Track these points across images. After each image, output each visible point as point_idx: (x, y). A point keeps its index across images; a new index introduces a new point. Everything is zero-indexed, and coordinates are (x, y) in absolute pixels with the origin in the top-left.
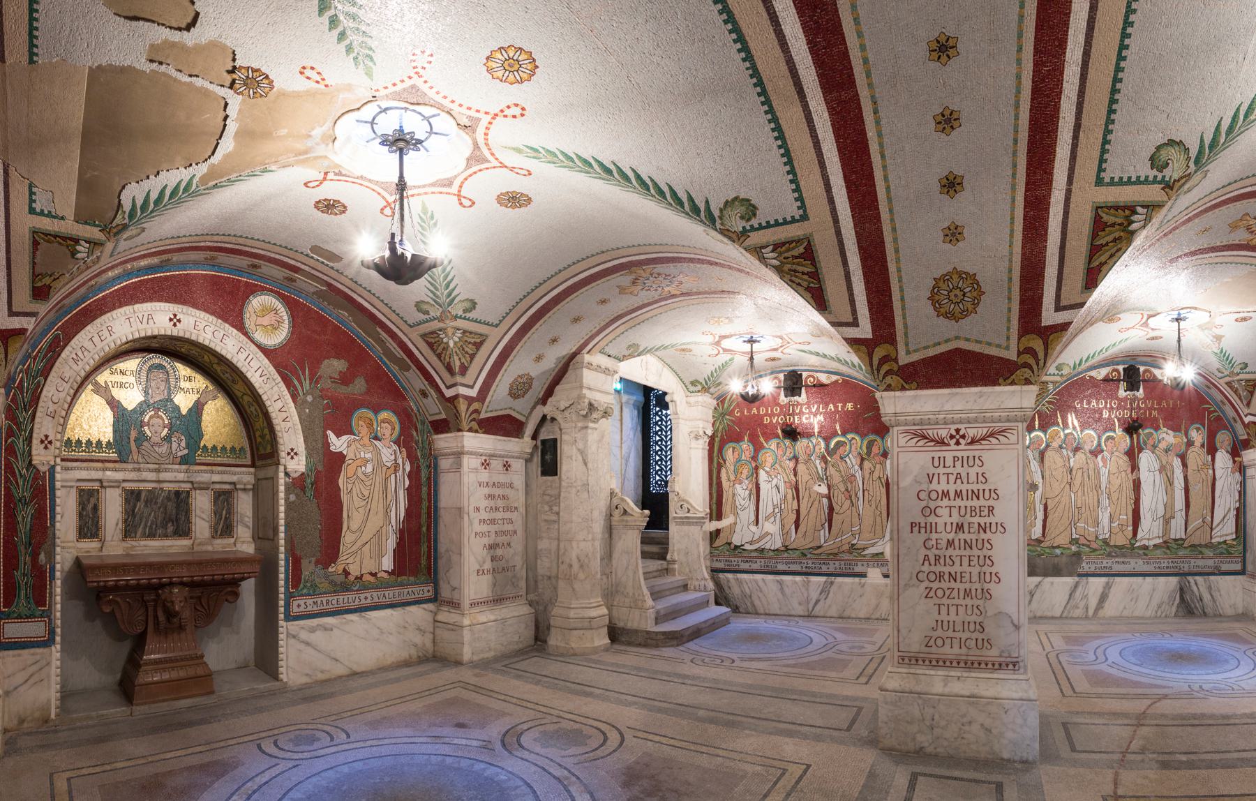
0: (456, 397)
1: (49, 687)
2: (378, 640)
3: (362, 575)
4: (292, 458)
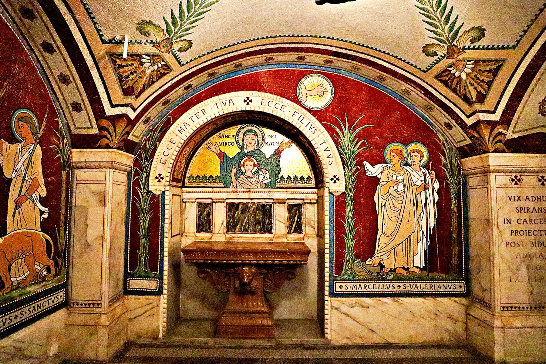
0: (479, 122)
1: (158, 319)
2: (411, 320)
3: (395, 269)
4: (335, 182)
